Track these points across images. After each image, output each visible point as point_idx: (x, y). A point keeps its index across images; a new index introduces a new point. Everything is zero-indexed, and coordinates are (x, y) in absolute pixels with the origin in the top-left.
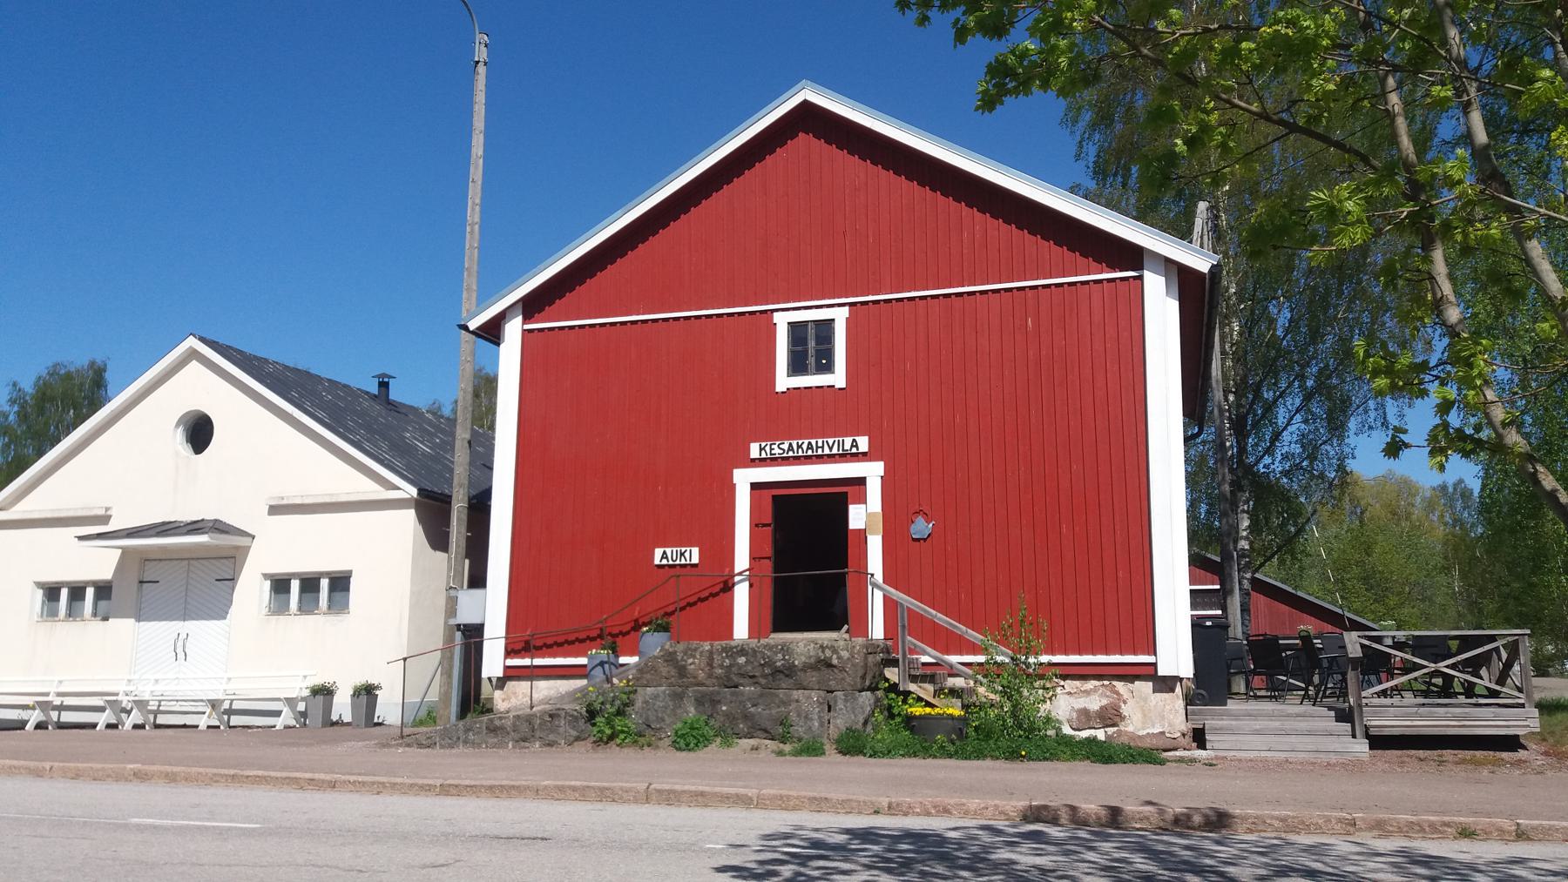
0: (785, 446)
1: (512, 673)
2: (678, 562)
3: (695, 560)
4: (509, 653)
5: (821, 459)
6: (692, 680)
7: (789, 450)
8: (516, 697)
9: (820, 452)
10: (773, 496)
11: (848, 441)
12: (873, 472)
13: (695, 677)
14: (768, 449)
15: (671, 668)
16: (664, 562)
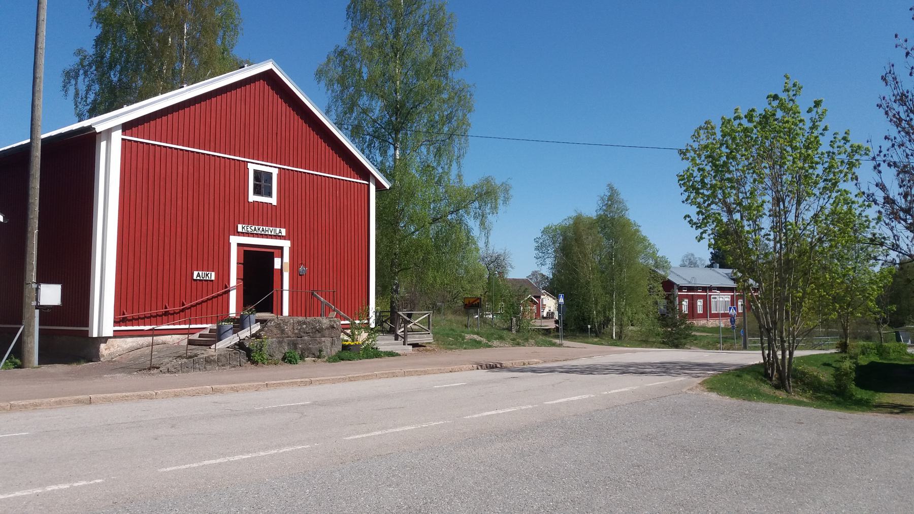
0: (253, 228)
1: (118, 334)
2: (205, 279)
3: (213, 278)
4: (116, 323)
5: (267, 236)
6: (286, 335)
7: (254, 230)
8: (113, 347)
9: (267, 233)
10: (244, 250)
11: (278, 230)
12: (286, 244)
13: (287, 334)
14: (245, 228)
15: (278, 331)
16: (198, 278)
